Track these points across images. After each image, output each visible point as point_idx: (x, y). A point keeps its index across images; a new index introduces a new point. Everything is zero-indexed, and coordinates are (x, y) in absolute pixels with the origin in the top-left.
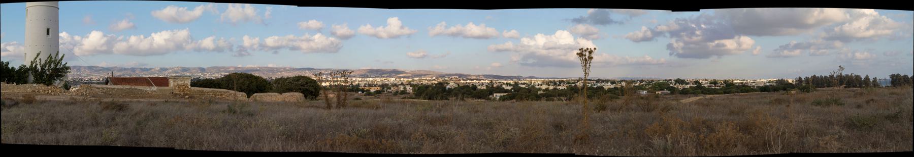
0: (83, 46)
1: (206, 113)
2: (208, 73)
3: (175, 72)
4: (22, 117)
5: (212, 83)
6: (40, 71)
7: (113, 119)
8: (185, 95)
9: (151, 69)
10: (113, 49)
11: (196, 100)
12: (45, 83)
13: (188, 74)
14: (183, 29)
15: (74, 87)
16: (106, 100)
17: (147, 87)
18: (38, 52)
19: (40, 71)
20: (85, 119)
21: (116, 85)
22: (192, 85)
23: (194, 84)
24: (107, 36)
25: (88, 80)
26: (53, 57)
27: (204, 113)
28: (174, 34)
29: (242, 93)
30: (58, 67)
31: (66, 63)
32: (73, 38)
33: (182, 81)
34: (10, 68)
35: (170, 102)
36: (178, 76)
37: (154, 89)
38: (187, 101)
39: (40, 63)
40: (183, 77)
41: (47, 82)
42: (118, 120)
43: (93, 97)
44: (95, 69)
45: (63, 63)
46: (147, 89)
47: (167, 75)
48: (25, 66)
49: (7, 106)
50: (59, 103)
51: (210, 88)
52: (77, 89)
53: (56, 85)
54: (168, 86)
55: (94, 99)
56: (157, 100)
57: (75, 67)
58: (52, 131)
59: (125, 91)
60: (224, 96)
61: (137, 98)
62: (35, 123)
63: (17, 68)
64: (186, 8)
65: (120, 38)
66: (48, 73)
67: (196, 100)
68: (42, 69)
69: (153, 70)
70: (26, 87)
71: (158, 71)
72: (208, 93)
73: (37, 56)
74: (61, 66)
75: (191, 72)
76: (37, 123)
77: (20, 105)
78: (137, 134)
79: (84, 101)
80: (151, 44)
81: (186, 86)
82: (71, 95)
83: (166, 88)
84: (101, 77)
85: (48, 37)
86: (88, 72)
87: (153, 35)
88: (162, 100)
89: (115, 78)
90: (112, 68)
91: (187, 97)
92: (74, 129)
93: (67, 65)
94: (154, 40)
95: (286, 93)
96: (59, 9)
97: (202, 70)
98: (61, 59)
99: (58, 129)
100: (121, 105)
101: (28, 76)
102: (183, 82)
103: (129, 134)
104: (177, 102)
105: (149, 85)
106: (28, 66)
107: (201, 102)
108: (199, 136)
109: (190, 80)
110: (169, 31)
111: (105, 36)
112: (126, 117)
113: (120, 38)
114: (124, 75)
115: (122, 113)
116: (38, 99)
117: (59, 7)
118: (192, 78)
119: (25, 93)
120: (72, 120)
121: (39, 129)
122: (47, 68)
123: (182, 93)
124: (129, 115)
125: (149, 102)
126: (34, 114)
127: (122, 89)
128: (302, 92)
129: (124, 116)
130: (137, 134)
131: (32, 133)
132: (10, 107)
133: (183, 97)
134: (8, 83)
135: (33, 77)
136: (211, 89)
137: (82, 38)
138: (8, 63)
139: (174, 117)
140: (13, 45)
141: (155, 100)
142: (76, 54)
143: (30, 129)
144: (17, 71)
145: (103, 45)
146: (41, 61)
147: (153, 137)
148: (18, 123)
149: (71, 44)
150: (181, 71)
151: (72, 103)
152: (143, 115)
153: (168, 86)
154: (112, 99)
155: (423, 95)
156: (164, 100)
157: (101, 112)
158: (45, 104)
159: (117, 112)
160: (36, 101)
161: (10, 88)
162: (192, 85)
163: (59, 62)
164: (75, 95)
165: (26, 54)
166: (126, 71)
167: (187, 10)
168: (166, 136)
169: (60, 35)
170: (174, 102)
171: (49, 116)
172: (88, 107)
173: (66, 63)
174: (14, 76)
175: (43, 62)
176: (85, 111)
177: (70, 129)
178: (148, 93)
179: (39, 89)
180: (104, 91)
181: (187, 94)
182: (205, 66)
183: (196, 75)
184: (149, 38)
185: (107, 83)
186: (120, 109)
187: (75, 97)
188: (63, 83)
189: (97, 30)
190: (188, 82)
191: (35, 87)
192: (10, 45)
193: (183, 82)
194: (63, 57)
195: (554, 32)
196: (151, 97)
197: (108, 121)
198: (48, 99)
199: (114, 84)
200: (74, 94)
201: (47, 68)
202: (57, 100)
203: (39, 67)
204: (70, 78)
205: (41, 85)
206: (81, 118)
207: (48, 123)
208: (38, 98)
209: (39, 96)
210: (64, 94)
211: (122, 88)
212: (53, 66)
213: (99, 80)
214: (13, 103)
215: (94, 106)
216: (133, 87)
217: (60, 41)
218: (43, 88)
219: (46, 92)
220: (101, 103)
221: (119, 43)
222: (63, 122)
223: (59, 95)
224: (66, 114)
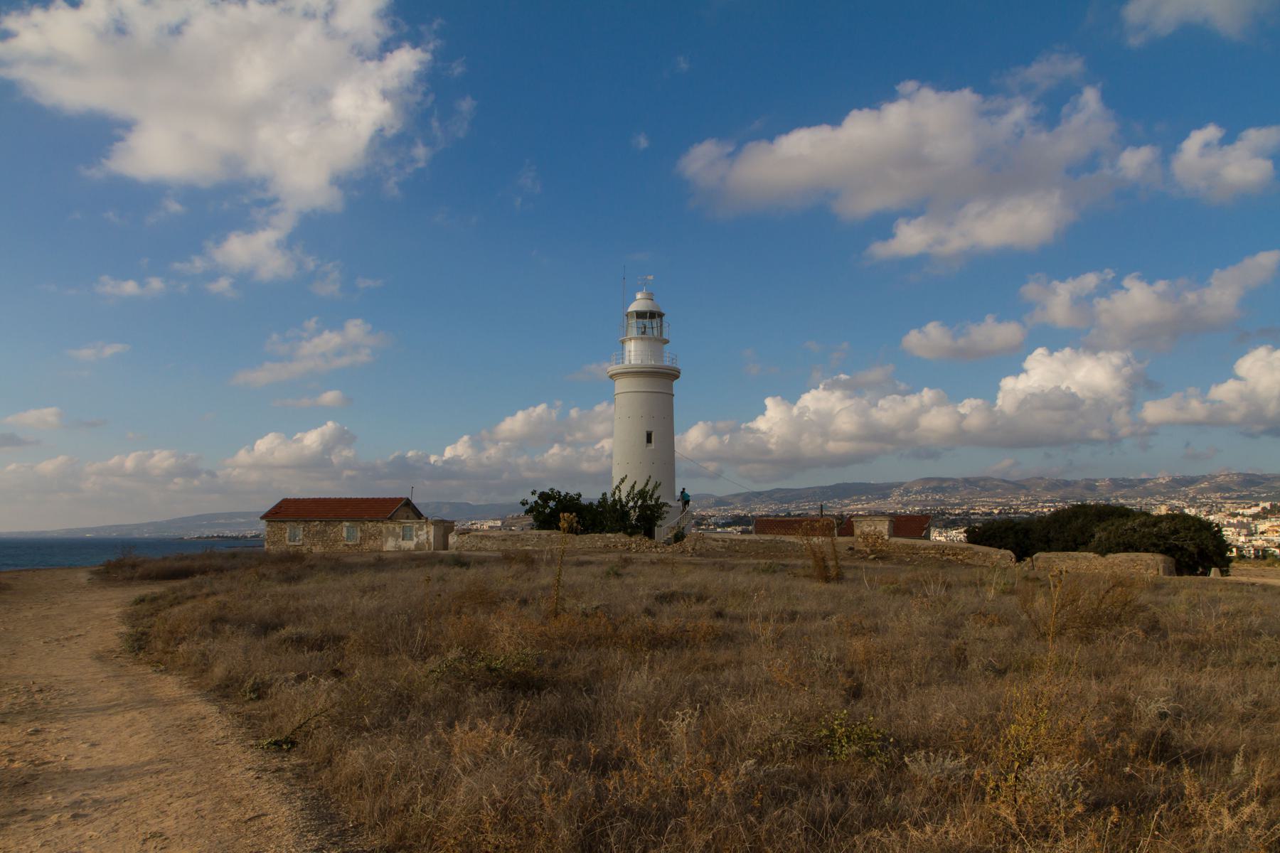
12: (626, 532)
21: (764, 533)
25: (959, 514)
29: (1002, 551)
33: (870, 526)
60: (960, 557)
71: (1165, 485)
72: (925, 549)
81: (880, 536)
95: (1118, 555)
97: (1090, 486)
102: (873, 528)
127: (756, 542)
128: (1161, 552)
153: (839, 535)
180: (727, 545)
191: (609, 538)
193: (873, 528)
195: (799, 397)
205: (620, 534)
213: (991, 514)
216: (778, 538)
217: (676, 455)
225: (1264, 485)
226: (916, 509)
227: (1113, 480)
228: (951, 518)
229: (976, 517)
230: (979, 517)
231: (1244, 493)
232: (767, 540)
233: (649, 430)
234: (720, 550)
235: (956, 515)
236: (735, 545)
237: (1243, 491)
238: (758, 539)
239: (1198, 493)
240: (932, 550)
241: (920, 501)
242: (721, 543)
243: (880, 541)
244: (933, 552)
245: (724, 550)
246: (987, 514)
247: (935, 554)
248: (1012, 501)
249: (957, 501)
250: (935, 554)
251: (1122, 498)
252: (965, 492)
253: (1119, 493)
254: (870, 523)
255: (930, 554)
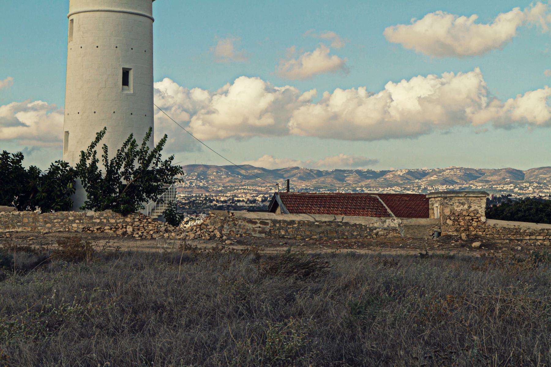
0: (214, 116)
1: (527, 287)
2: (531, 183)
3: (446, 181)
4: (57, 296)
5: (541, 211)
6: (103, 176)
7: (290, 299)
8: (473, 241)
9: (383, 173)
10: (290, 124)
11: (500, 255)
12: (116, 209)
13: (479, 186)
14: (466, 72)
15: (192, 219)
16: (270, 251)
17: (375, 219)
18: (100, 129)
19: (103, 176)
20: (218, 300)
22: (489, 215)
23: (492, 213)
24: (275, 91)
25: (225, 202)
26: (139, 143)
27: (521, 286)
28: (443, 84)
30: (150, 168)
31: (172, 158)
32: (188, 94)
34: (27, 168)
35: (432, 257)
36: (452, 192)
37: (392, 225)
38: (477, 254)
39: (105, 157)
40: (467, 193)
41: (122, 207)
42: (300, 302)
43: (240, 243)
44: (243, 172)
45: (164, 156)
46: (375, 222)
47: (425, 189)
48: (66, 165)
49: (18, 268)
50: (152, 258)
51: (537, 222)
52: (199, 222)
53: (145, 212)
54: (427, 216)
55: (240, 247)
56: (403, 252)
57: (192, 167)
58: (133, 330)
59: (320, 230)
61: (350, 246)
62: (89, 311)
63: (44, 169)
64: (474, 17)
65: (307, 95)
66: (124, 182)
67: (500, 255)
68: (110, 172)
69: (389, 176)
70: (67, 218)
71: (402, 177)
72: (531, 234)
73: (98, 139)
74: (160, 165)
75: (487, 181)
76: (97, 312)
77: (51, 266)
78: (352, 338)
79: (216, 254)
80: (385, 112)
81: (475, 216)
82: (184, 239)
83: (422, 221)
84: (259, 192)
85: (126, 92)
86: (226, 180)
87: (390, 86)
88: (413, 253)
89: (293, 195)
90: (286, 170)
91: (476, 244)
92: (190, 323)
93: (174, 163)
94: (392, 100)
96: (153, 20)
98: (160, 147)
99: (151, 326)
100: (309, 263)
101: (72, 191)
102: (466, 207)
103: (333, 339)
104: (452, 258)
105: (382, 213)
106: (74, 163)
107: (513, 258)
108: (519, 345)
109: (485, 200)
110: (430, 76)
111: (268, 90)
112: (322, 293)
113: (307, 95)
114: (316, 188)
115: (311, 285)
116: (98, 249)
117: (154, 16)
118: (490, 197)
119: (66, 235)
120: (186, 301)
121: (100, 326)
122: (122, 169)
123: (464, 236)
124: (328, 290)
125: (379, 255)
126: (89, 287)
127: (310, 224)
129: (316, 291)
130: (352, 338)
131: (82, 335)
132: (26, 269)
133: (466, 244)
134: (19, 209)
135: (86, 194)
136: (540, 226)
137: (212, 94)
138: (20, 157)
139: (443, 296)
140: (34, 109)
141: (393, 252)
142: (198, 136)
143: (77, 325)
144: (45, 177)
145: (263, 113)
146: (106, 152)
147: (393, 346)
148: (47, 311)
149: (185, 110)
150: (460, 178)
151: (186, 259)
152: (364, 289)
153: (427, 216)
154: (285, 249)
155: (340, 283)
156: (417, 252)
157: (258, 282)
158: (117, 261)
159: (300, 282)
160: (94, 254)
161: (26, 220)
162: (489, 215)
163: (152, 156)
164: (195, 239)
165: (67, 133)
166: (322, 179)
167: (476, 22)
168: (427, 343)
169: (157, 85)
170: (443, 257)
171: (126, 293)
172: (226, 268)
173: (172, 158)
174: (36, 191)
175: (112, 155)
176: (220, 280)
177: (181, 325)
178: (377, 234)
179: (101, 223)
180: (267, 229)
181: (476, 238)
182: (524, 168)
183: (499, 188)
184: (381, 94)
185: (274, 207)
186: (306, 275)
187: (194, 244)
188: (163, 208)
189: (249, 76)
190: (480, 207)
191: (92, 217)
192: (26, 110)
193: (466, 207)
194: (163, 142)
196: (383, 245)
197: (275, 305)
198: (124, 249)
199: (292, 212)
200: (192, 236)
201: (122, 169)
202: (147, 250)
203: (101, 168)
204: (181, 196)
205: (108, 213)
206: (208, 296)
207: (123, 310)
208: (99, 246)
209: (102, 243)
210: (166, 235)
211: (312, 220)
212: (137, 165)
213: (254, 201)
214: (35, 259)
215: (242, 266)
216: (339, 218)
217: (157, 102)
218: (112, 221)
219: (120, 232)
220: (258, 257)
221: (303, 109)
222: (163, 306)
223: (152, 238)
224: (169, 288)
225: (480, 179)
226: (182, 195)
227: (410, 173)
228: (218, 205)
229: (241, 204)
230: (245, 204)
231: (464, 186)
232: (325, 222)
233: (127, 66)
234: (258, 235)
235: (222, 202)
236: (279, 229)
237: (463, 184)
238: (313, 220)
239: (428, 185)
240: (540, 235)
241: (185, 187)
242: (258, 225)
243: (475, 224)
244: (541, 238)
245: (263, 235)
246: (251, 202)
247: (544, 240)
248: (271, 189)
249: (220, 189)
250: (544, 240)
251: (367, 188)
252: (227, 180)
253: (363, 184)
254: (463, 200)
255: (537, 240)
